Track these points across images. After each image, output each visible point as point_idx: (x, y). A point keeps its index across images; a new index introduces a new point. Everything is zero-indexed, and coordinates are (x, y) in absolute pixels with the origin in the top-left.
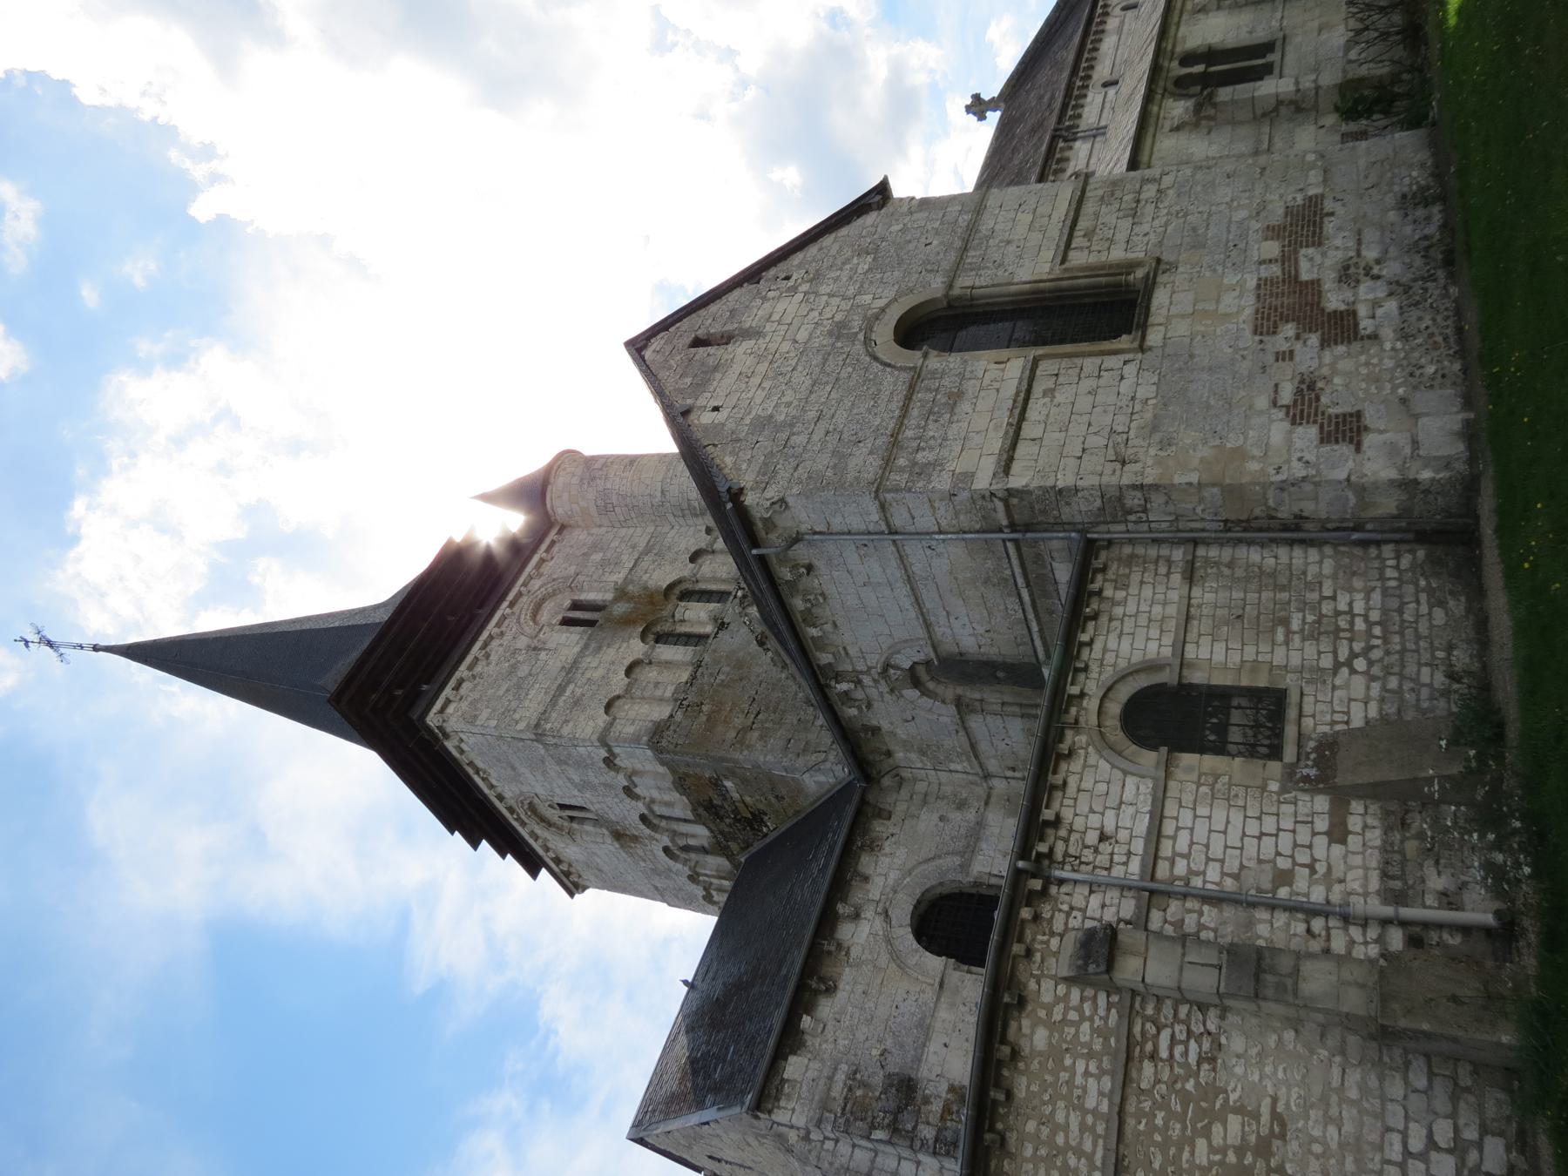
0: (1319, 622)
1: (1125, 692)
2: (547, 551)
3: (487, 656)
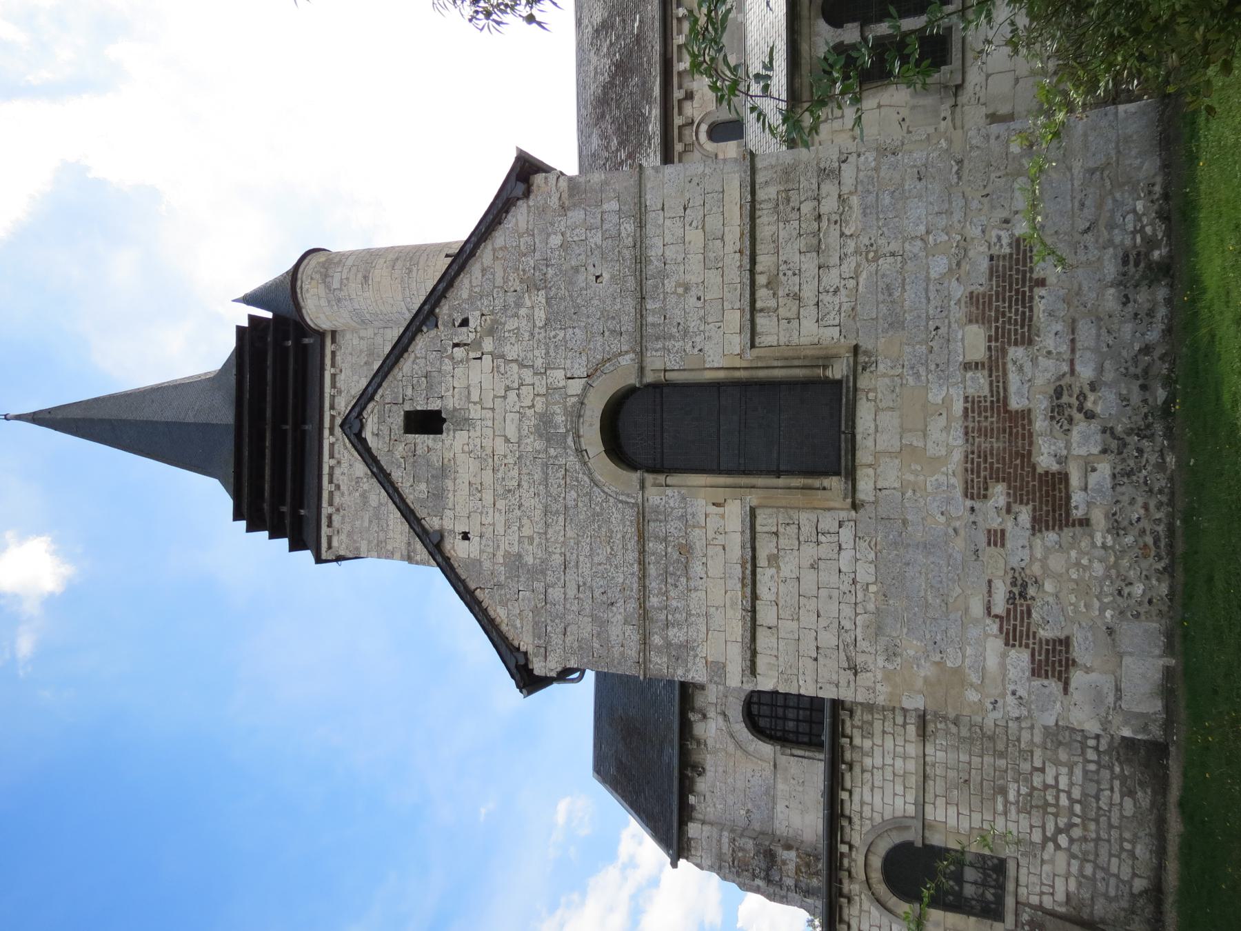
0: (1030, 795)
1: (883, 847)
2: (333, 365)
3: (338, 487)
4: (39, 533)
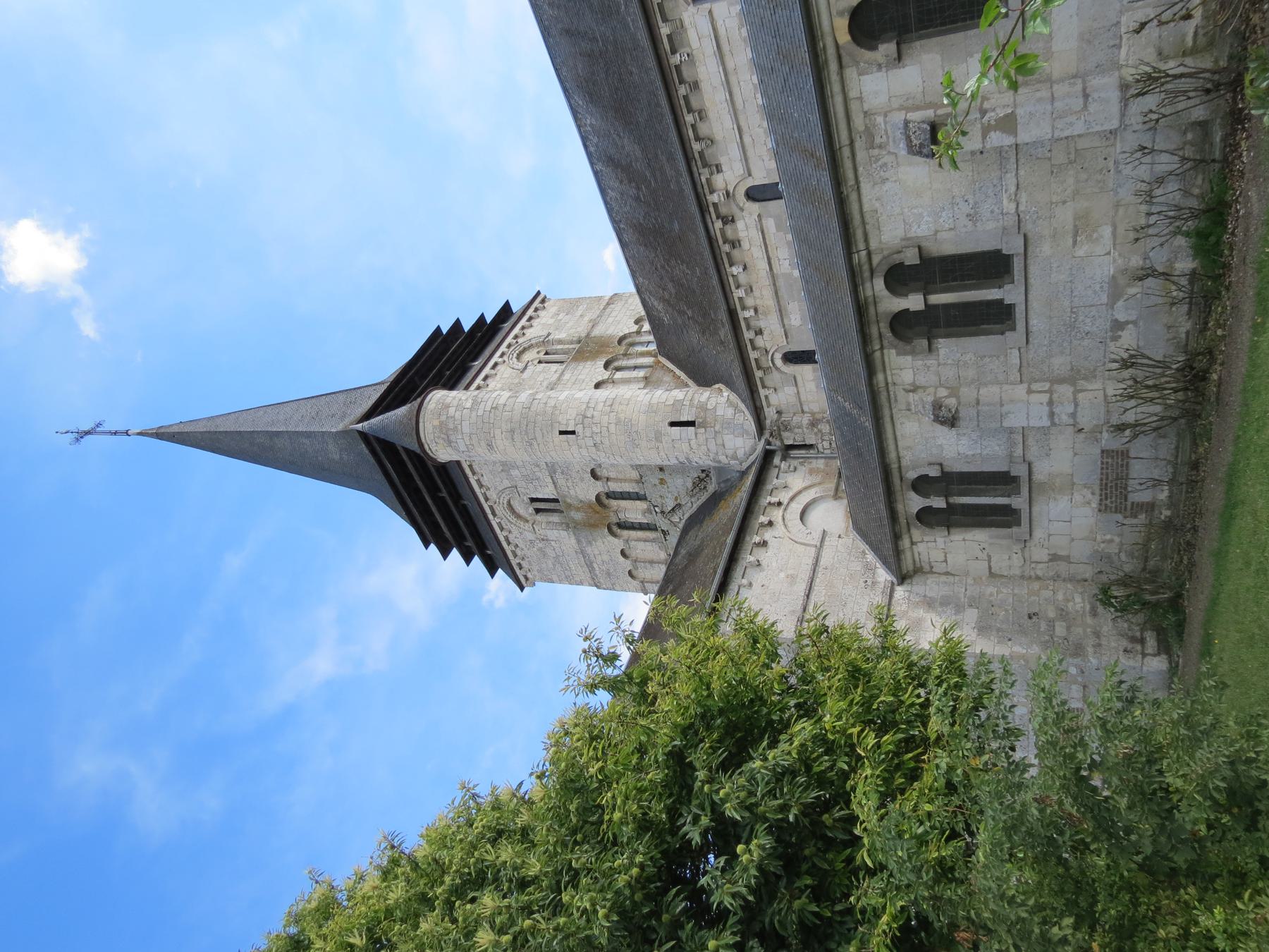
2: (474, 473)
3: (517, 546)
4: (24, 214)
